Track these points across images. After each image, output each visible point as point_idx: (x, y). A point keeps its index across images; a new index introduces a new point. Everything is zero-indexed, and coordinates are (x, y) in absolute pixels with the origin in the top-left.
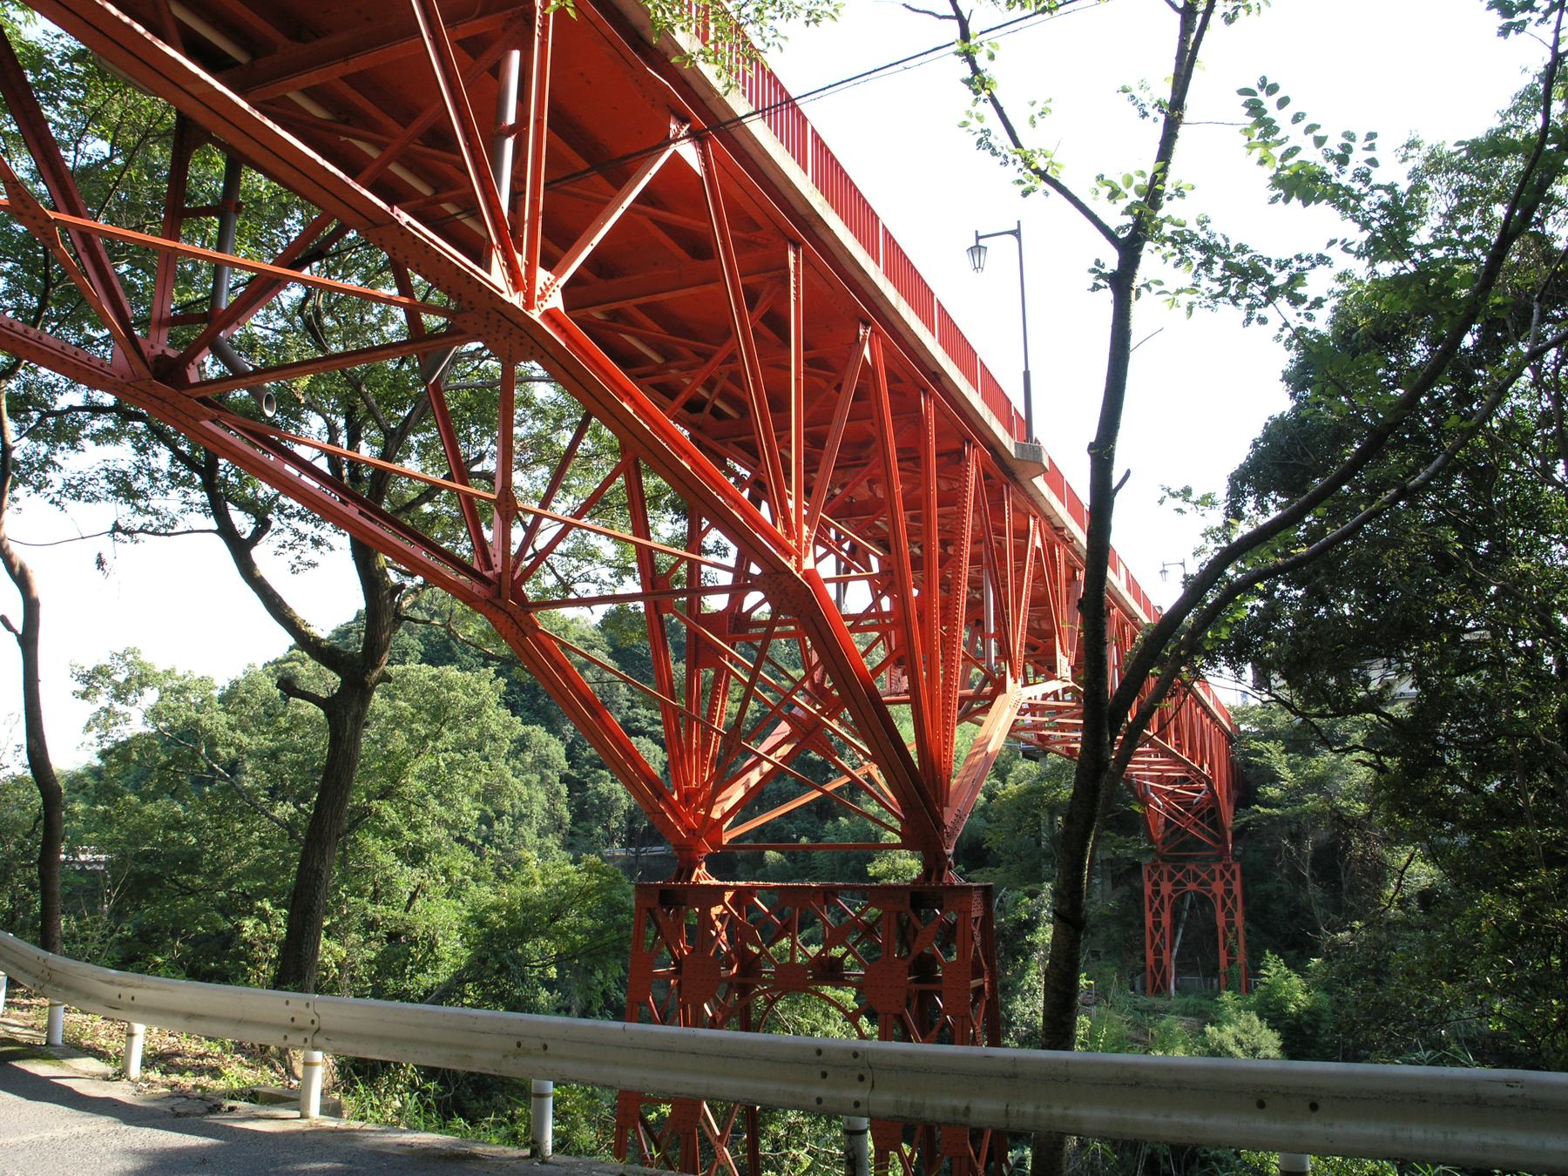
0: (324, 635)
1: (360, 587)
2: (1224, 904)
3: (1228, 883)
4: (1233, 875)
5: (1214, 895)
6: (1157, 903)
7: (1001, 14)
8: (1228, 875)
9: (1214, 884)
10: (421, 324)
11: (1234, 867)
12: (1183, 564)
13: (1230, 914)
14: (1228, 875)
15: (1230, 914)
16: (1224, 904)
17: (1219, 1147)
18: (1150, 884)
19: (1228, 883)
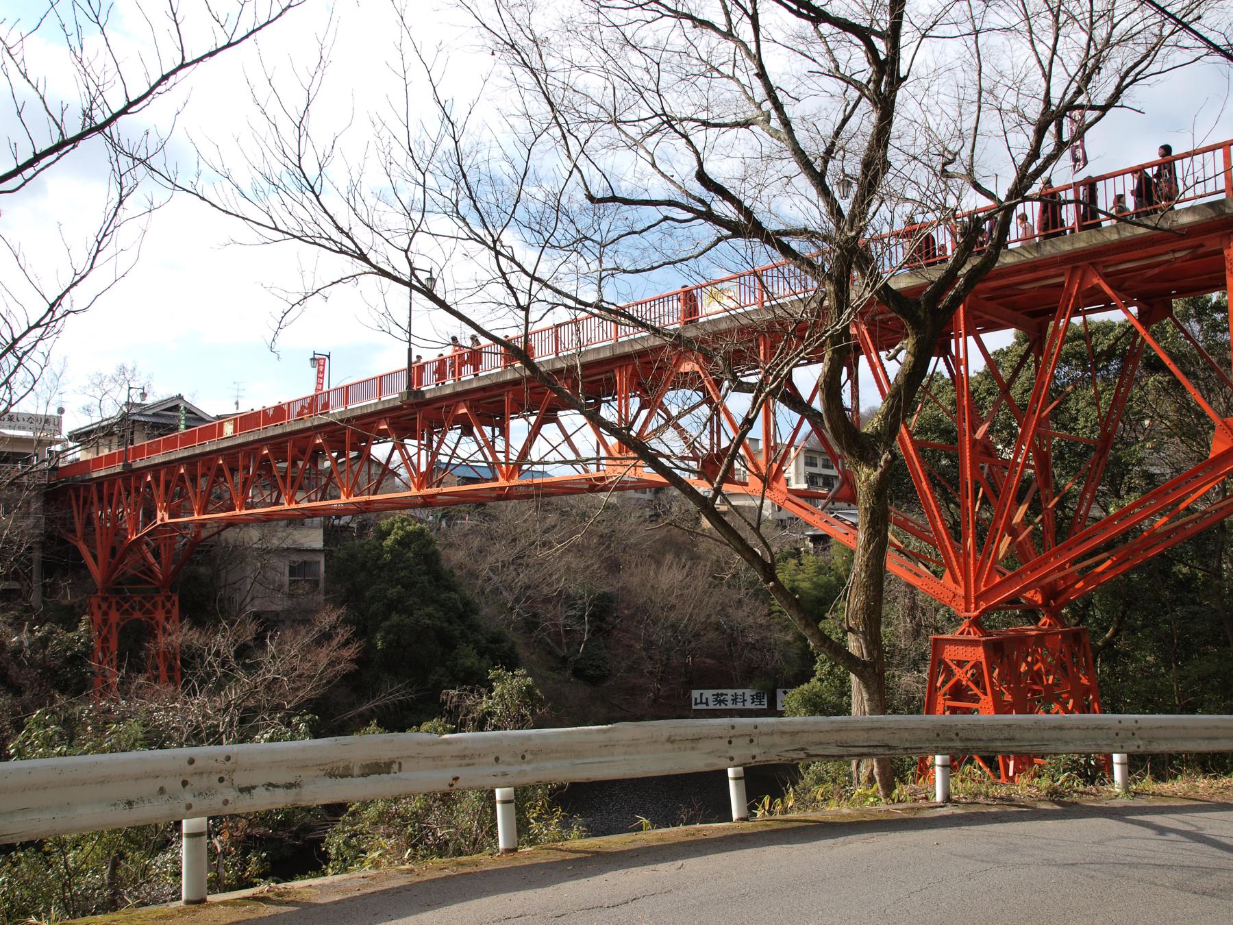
4: (173, 605)
14: (168, 605)
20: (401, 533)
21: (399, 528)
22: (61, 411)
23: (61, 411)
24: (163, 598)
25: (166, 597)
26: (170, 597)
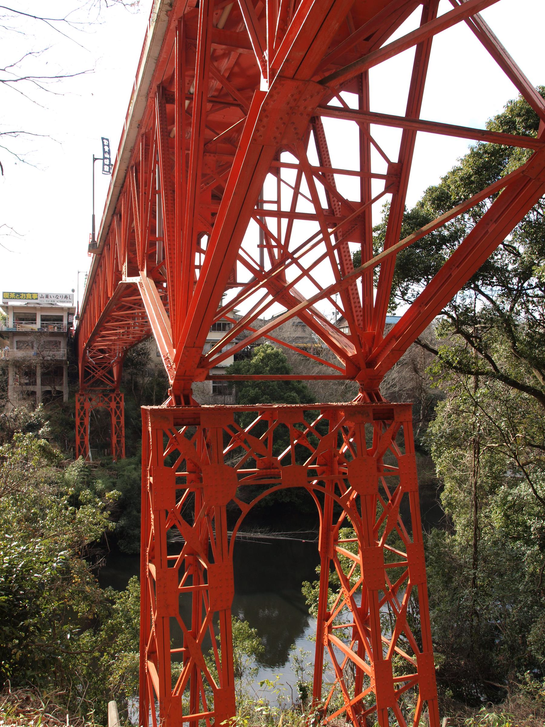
0: (518, 100)
1: (414, 11)
2: (116, 413)
3: (118, 403)
4: (121, 399)
5: (112, 409)
6: (82, 413)
7: (113, 2)
8: (118, 399)
9: (111, 403)
10: (335, 245)
11: (121, 395)
12: (95, 159)
13: (119, 418)
14: (118, 399)
15: (119, 418)
16: (116, 413)
17: (94, 235)
18: (79, 403)
19: (118, 403)
20: (263, 354)
21: (263, 352)
22: (73, 291)
23: (73, 291)
24: (115, 395)
25: (117, 394)
26: (119, 394)
